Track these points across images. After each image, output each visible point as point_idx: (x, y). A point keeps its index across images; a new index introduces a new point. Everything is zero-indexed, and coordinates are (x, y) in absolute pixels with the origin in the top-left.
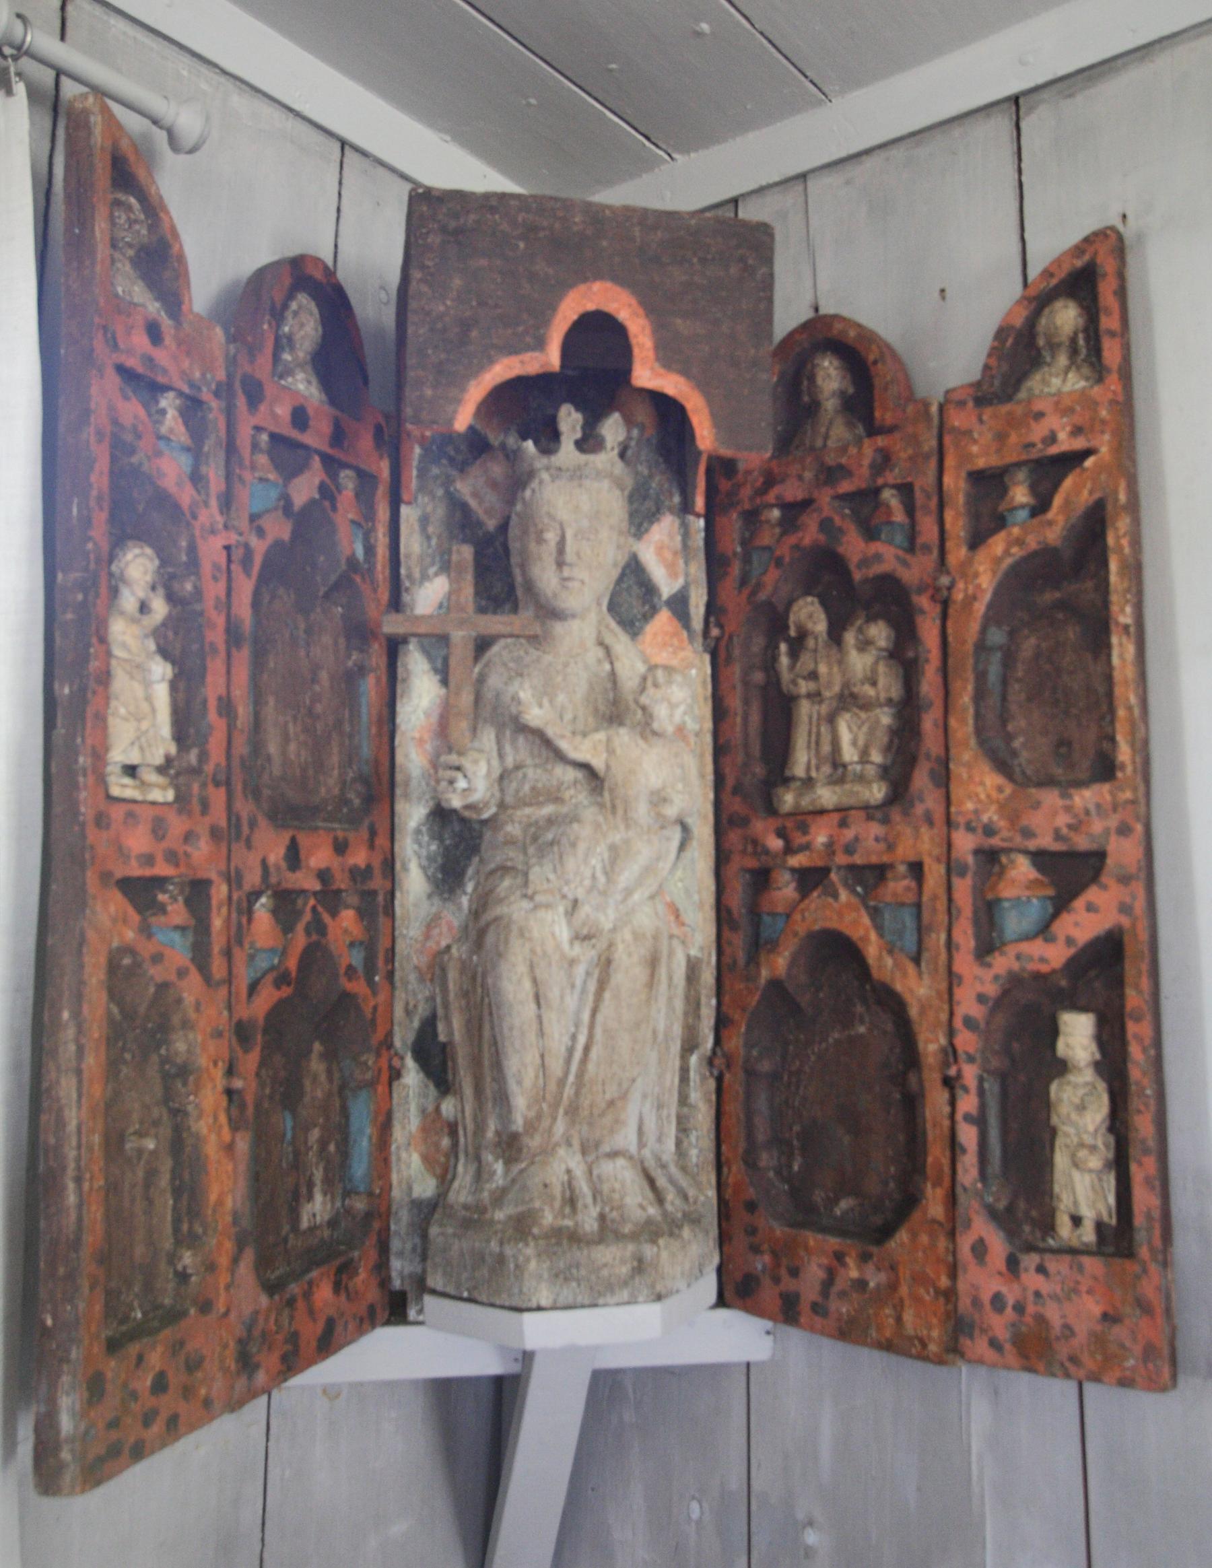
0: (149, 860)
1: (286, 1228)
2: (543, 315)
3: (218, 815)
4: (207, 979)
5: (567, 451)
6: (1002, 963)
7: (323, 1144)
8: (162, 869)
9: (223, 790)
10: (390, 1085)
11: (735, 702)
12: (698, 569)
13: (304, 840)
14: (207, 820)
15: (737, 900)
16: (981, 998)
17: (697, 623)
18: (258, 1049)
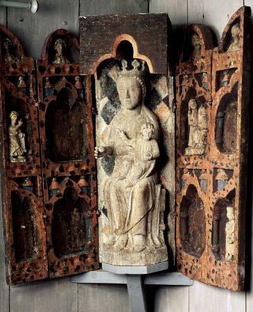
0: (20, 174)
1: (68, 246)
2: (110, 44)
3: (38, 163)
4: (37, 195)
5: (124, 71)
6: (217, 195)
7: (79, 230)
8: (23, 175)
9: (39, 158)
10: (97, 219)
11: (178, 125)
12: (171, 90)
13: (65, 166)
14: (35, 164)
15: (178, 176)
16: (213, 203)
17: (171, 106)
18: (52, 210)
